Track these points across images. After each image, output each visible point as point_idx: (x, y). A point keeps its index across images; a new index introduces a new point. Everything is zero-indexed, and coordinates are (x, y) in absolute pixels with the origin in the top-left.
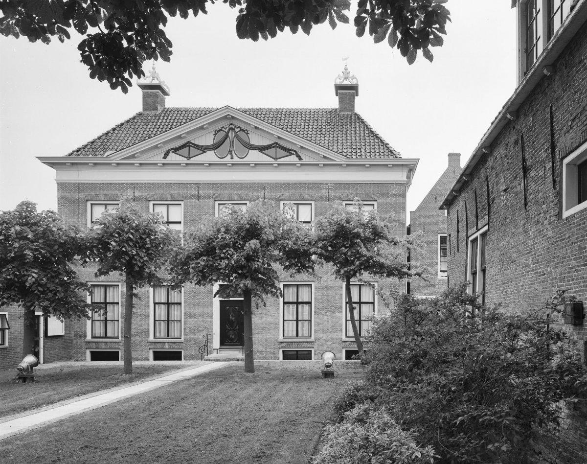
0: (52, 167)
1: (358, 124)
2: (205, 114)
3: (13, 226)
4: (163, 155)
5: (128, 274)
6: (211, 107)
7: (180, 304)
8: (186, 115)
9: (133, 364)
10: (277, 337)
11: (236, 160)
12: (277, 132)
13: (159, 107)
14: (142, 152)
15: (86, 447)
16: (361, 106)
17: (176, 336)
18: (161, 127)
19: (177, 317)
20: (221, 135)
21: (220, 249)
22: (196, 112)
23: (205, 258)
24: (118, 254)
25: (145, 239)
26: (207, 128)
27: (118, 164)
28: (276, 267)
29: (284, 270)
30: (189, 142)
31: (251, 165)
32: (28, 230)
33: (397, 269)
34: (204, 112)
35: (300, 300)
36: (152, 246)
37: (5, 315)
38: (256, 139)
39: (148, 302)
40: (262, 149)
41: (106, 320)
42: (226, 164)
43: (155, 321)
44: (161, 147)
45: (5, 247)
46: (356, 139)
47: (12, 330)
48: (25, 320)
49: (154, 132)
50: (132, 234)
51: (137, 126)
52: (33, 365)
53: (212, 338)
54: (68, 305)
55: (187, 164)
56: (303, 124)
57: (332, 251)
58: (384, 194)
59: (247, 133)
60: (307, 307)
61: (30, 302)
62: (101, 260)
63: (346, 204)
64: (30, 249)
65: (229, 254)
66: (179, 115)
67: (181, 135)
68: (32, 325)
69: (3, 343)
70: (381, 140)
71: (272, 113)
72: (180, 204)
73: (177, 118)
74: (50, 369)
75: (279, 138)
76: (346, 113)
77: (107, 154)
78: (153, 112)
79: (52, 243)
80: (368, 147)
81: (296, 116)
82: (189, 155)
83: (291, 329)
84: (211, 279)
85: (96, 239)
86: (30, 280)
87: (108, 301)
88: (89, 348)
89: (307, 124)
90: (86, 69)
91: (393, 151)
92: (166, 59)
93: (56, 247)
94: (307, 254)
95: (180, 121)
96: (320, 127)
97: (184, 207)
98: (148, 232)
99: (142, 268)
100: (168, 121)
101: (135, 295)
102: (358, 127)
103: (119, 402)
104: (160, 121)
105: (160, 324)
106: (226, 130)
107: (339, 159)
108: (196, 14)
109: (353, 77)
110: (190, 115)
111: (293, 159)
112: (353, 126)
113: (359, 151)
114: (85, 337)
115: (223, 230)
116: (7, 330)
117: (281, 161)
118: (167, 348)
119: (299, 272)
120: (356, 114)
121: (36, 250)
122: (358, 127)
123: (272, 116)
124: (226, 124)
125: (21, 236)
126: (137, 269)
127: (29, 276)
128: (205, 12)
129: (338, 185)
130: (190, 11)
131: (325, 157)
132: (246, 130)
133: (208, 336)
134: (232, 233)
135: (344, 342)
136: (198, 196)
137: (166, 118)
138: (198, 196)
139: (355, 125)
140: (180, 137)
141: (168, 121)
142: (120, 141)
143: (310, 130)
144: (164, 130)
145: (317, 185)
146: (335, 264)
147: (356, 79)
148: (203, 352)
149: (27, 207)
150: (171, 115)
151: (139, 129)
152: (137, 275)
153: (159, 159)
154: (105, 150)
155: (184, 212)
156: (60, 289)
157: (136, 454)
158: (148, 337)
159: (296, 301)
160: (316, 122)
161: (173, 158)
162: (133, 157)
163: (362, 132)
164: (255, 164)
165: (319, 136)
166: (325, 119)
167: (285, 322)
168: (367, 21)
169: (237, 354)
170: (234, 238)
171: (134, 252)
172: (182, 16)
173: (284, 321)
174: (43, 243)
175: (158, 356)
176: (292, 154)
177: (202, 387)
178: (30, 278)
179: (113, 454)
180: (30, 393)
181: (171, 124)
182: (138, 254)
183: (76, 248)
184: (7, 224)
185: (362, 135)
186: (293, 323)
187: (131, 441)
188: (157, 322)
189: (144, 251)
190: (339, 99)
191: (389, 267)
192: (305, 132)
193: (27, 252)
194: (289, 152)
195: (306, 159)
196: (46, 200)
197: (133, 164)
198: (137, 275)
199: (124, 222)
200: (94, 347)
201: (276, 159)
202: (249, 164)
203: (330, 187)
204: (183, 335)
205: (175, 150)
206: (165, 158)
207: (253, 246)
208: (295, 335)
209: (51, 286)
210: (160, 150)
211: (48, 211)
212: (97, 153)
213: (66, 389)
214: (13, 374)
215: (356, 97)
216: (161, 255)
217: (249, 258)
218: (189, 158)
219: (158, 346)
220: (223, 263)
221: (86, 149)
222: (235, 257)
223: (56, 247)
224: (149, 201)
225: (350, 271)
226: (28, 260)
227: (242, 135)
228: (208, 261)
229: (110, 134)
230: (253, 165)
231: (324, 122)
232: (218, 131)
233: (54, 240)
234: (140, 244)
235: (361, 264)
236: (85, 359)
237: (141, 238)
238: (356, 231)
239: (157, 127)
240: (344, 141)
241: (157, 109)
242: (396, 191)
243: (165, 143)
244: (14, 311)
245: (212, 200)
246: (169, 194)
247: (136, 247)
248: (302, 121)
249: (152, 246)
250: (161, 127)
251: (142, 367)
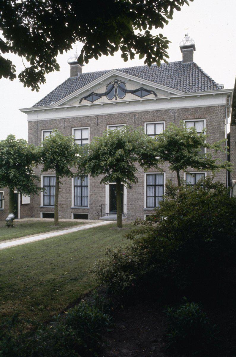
0: (26, 113)
1: (194, 69)
2: (103, 75)
3: (5, 147)
4: (79, 102)
5: (56, 170)
6: (106, 70)
7: (88, 186)
8: (93, 76)
9: (59, 220)
10: (143, 207)
11: (119, 100)
12: (142, 81)
13: (79, 74)
14: (68, 101)
15: (23, 257)
16: (197, 58)
17: (151, 206)
18: (79, 85)
19: (86, 194)
20: (111, 86)
21: (102, 155)
22: (98, 74)
23: (94, 161)
24: (52, 161)
25: (65, 151)
26: (102, 83)
27: (57, 109)
28: (136, 164)
29: (140, 166)
30: (93, 93)
31: (140, 101)
32: (11, 149)
33: (208, 164)
34: (102, 73)
35: (157, 184)
36: (68, 155)
37: (2, 193)
38: (129, 87)
39: (71, 185)
40: (133, 92)
41: (50, 196)
42: (112, 104)
43: (74, 196)
44: (78, 97)
45: (2, 158)
46: (192, 79)
47: (6, 200)
48: (10, 195)
49: (76, 88)
50: (58, 149)
51: (67, 86)
52: (12, 219)
53: (105, 206)
54: (30, 188)
55: (91, 105)
56: (159, 73)
57: (168, 154)
58: (211, 113)
59: (125, 84)
60: (161, 188)
61: (11, 186)
62: (45, 163)
63: (186, 122)
64: (12, 159)
65: (107, 158)
66: (89, 77)
67: (88, 89)
68: (14, 199)
69: (1, 207)
70: (209, 78)
71: (141, 69)
72: (88, 129)
73: (88, 79)
74: (23, 222)
75: (143, 84)
76: (187, 63)
77: (52, 104)
78: (75, 77)
79: (22, 155)
80: (200, 84)
81: (155, 69)
82: (93, 100)
83: (151, 202)
84: (97, 173)
85: (41, 153)
86: (12, 175)
87: (51, 185)
88: (42, 211)
89: (162, 73)
90: (22, 84)
91: (217, 85)
92: (58, 70)
93: (23, 157)
94: (152, 157)
95: (89, 80)
96: (170, 74)
97: (90, 130)
98: (67, 148)
99: (63, 168)
100: (83, 81)
101: (61, 183)
102: (194, 71)
103: (46, 239)
104: (79, 82)
105: (77, 198)
106: (113, 84)
107: (180, 94)
108: (66, 51)
109: (192, 40)
110: (95, 76)
111: (151, 96)
112: (191, 71)
113: (194, 87)
114: (40, 205)
115: (103, 144)
116: (3, 201)
117: (144, 98)
118: (80, 212)
119: (149, 167)
120: (194, 63)
121: (15, 159)
122: (194, 71)
123: (141, 71)
124: (113, 80)
125: (8, 153)
126: (60, 168)
127: (11, 173)
128: (72, 48)
129: (180, 110)
130: (64, 51)
131: (171, 94)
132: (124, 82)
133: (103, 205)
134: (109, 146)
135: (145, 210)
136: (98, 123)
137: (82, 79)
138: (98, 123)
139: (193, 70)
140: (88, 90)
141: (83, 81)
142: (58, 96)
143: (164, 76)
144: (81, 86)
145: (166, 111)
146: (170, 162)
147: (193, 40)
148: (100, 215)
149: (11, 137)
150: (85, 77)
151: (68, 88)
152: (61, 171)
153: (77, 104)
154: (50, 102)
155: (90, 132)
156: (25, 179)
157: (42, 262)
158: (71, 205)
159: (154, 184)
160: (168, 71)
161: (85, 102)
162: (64, 104)
163: (197, 74)
164: (129, 102)
165: (169, 80)
166: (173, 68)
167: (148, 198)
168: (128, 55)
169: (115, 216)
170: (110, 149)
171: (59, 159)
172: (61, 54)
173: (147, 197)
174: (18, 156)
175: (77, 216)
176: (151, 93)
177: (89, 234)
178: (11, 174)
179: (33, 261)
180: (10, 232)
181: (84, 82)
182: (61, 160)
183: (32, 158)
184: (2, 147)
185: (197, 76)
186: (152, 198)
187: (43, 256)
188: (76, 197)
189: (64, 158)
190: (183, 54)
191: (202, 163)
192: (161, 78)
193: (11, 161)
194: (149, 92)
195: (160, 96)
196: (21, 134)
197: (63, 108)
198: (61, 171)
199: (54, 142)
200: (44, 210)
201: (141, 97)
202: (126, 102)
203: (175, 112)
204: (89, 205)
205: (85, 98)
206: (80, 103)
207: (120, 153)
208: (153, 206)
209: (21, 178)
210: (77, 99)
211: (20, 139)
212: (47, 104)
213: (26, 231)
214: (5, 223)
215: (194, 52)
216: (73, 160)
217: (118, 160)
218: (92, 102)
219: (76, 210)
220: (103, 163)
221: (42, 102)
222: (110, 160)
223: (23, 157)
224: (144, 122)
225: (178, 166)
226: (11, 165)
227: (121, 85)
228: (95, 162)
229: (53, 92)
230: (142, 101)
231: (173, 70)
232: (108, 85)
233: (23, 154)
234: (62, 154)
235: (184, 162)
236: (39, 217)
237: (63, 151)
238: (181, 141)
239: (77, 85)
240: (185, 82)
241: (77, 75)
242: (219, 111)
243: (80, 95)
244: (5, 191)
245: (105, 125)
246: (81, 123)
247: (60, 155)
248: (159, 71)
249: (68, 155)
250: (79, 85)
251: (62, 222)
